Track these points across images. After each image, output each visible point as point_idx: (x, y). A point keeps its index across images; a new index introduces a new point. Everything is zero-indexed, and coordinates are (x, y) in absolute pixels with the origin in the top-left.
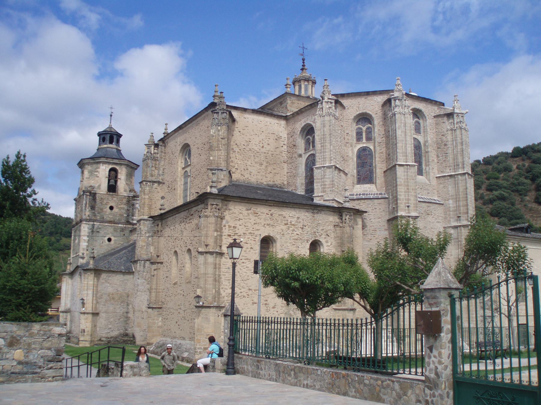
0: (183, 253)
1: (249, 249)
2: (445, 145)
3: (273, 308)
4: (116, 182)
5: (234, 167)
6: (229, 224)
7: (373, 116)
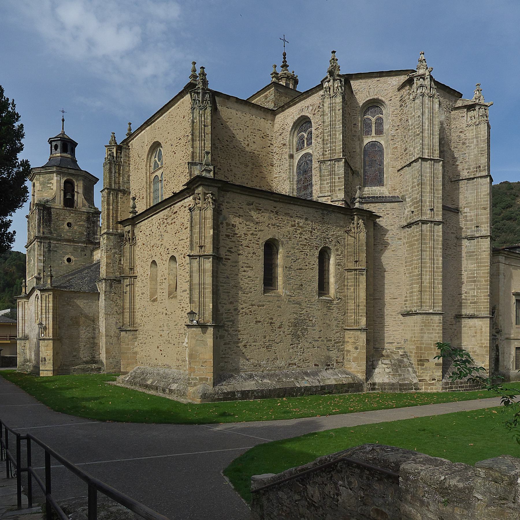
0: (164, 262)
2: (464, 143)
3: (279, 328)
4: (73, 196)
6: (227, 221)
7: (387, 102)
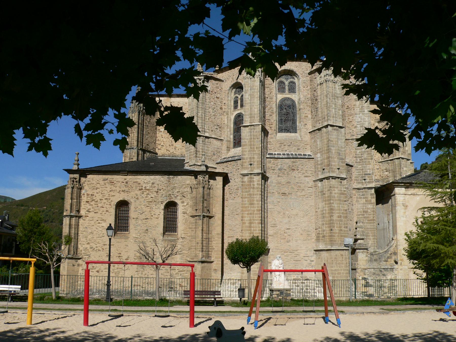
1: (105, 212)
5: (160, 145)
6: (88, 192)
